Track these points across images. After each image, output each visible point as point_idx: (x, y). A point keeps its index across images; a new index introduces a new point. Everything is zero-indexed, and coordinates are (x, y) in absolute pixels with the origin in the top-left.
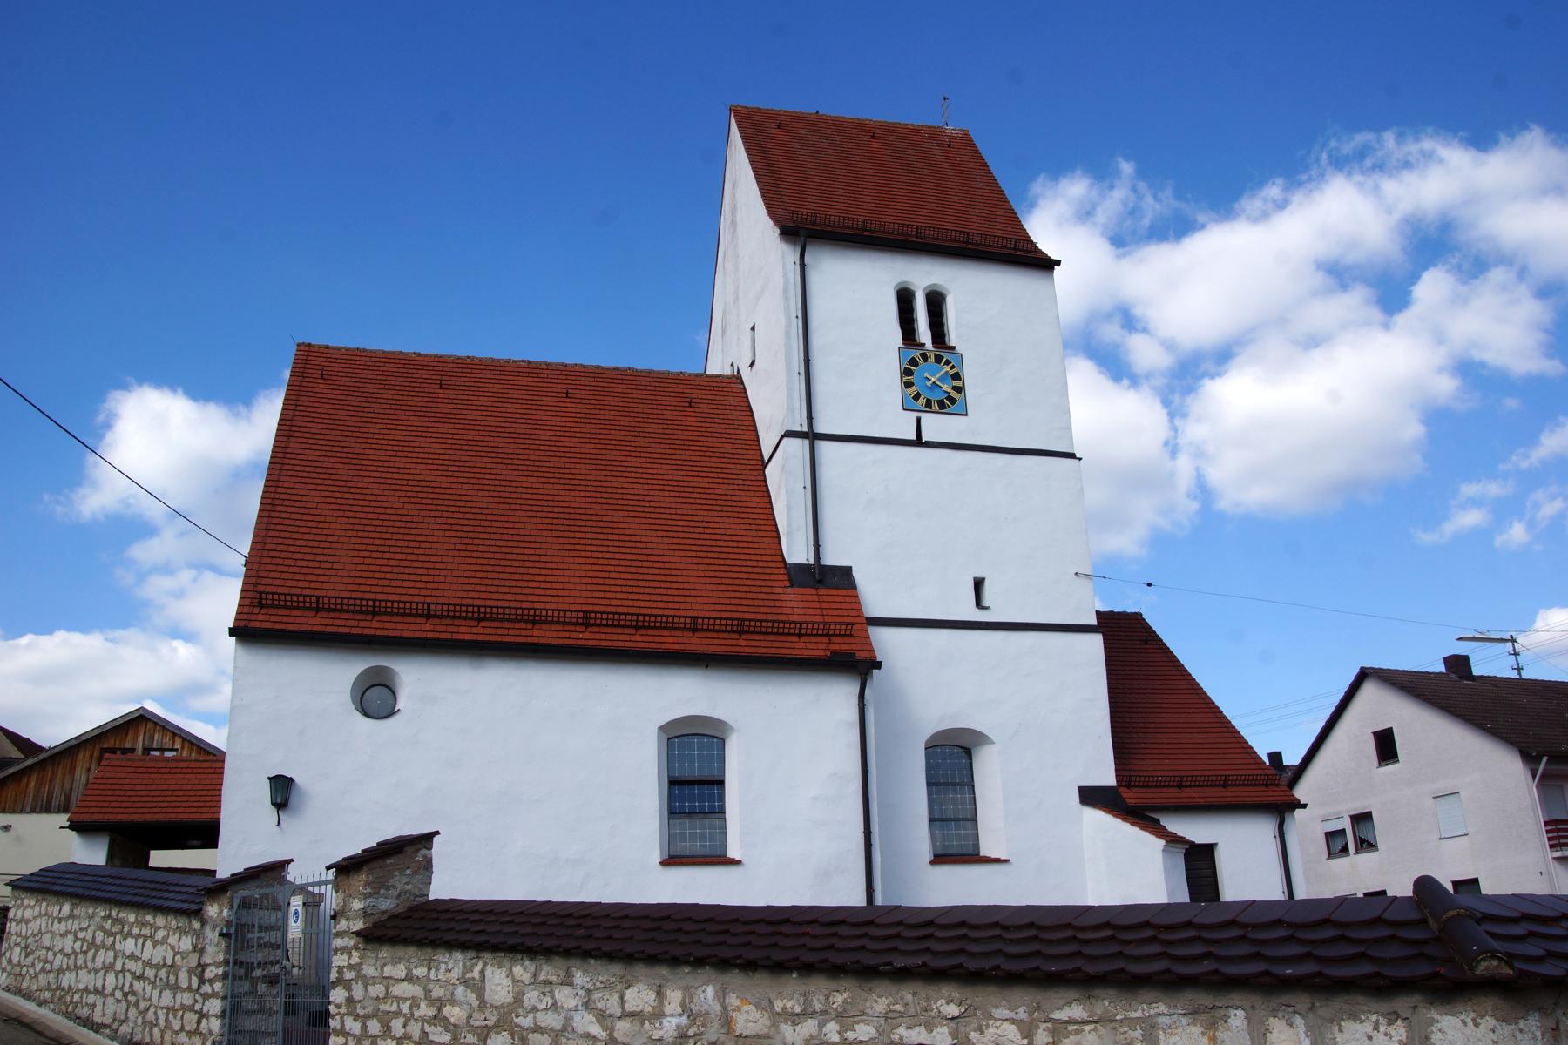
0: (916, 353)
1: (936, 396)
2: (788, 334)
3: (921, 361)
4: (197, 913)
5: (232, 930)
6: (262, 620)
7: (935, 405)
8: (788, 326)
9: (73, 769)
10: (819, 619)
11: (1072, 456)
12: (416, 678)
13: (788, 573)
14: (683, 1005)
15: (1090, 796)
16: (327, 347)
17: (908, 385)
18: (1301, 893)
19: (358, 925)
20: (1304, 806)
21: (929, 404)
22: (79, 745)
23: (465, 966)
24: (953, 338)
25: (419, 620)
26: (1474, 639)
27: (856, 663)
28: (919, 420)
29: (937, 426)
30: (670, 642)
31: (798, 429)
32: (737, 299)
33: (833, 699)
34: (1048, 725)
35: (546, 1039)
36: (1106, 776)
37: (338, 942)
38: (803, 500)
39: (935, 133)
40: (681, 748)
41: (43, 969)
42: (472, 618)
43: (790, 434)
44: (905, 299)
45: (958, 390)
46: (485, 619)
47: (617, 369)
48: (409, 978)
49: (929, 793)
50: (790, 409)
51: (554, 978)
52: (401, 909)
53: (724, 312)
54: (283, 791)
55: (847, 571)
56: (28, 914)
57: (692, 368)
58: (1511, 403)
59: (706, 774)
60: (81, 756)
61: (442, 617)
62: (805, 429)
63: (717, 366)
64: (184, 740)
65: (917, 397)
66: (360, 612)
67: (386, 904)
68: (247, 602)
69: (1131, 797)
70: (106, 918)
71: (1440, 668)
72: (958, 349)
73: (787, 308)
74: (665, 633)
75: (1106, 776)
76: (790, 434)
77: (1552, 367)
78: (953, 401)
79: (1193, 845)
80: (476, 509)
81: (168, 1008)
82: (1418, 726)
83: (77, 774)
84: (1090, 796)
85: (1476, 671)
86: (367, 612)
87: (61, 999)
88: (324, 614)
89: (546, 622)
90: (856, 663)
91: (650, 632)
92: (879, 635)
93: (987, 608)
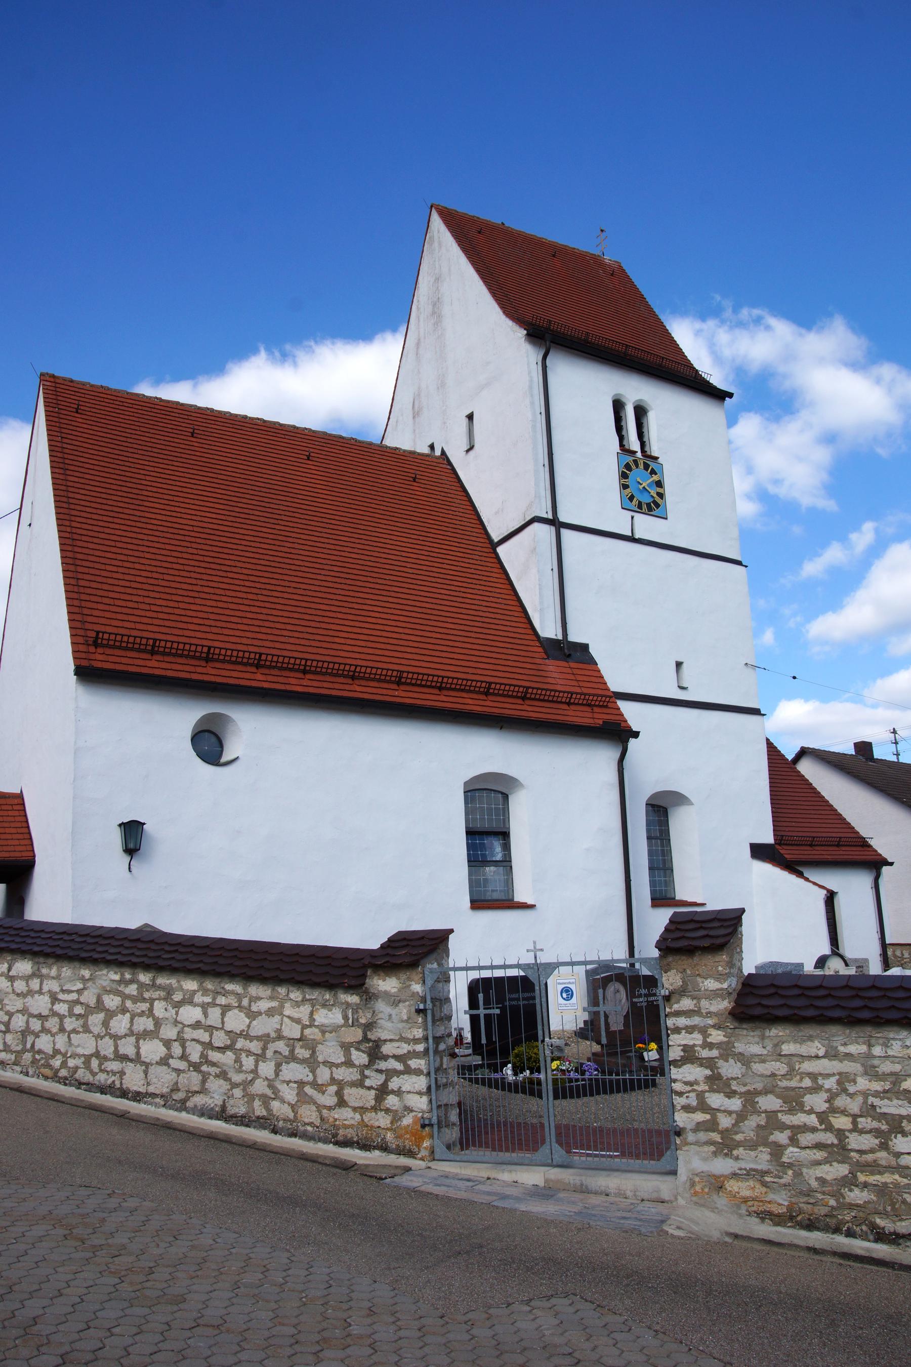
0: (630, 459)
1: (646, 499)
2: (534, 427)
3: (633, 467)
4: (357, 985)
5: (429, 1005)
6: (101, 659)
10: (578, 690)
12: (254, 730)
13: (542, 646)
15: (759, 852)
16: (72, 381)
17: (625, 487)
19: (725, 1005)
20: (891, 864)
21: (640, 505)
25: (249, 669)
29: (646, 526)
30: (471, 703)
31: (545, 516)
32: (442, 385)
33: (598, 759)
36: (767, 837)
44: (618, 406)
45: (661, 495)
46: (310, 672)
49: (649, 845)
58: (797, 530)
61: (270, 667)
62: (550, 516)
65: (631, 498)
69: (788, 853)
70: (122, 981)
73: (532, 403)
75: (767, 837)
77: (830, 505)
78: (658, 506)
81: (301, 1084)
84: (759, 852)
86: (200, 658)
90: (619, 734)
92: (622, 704)
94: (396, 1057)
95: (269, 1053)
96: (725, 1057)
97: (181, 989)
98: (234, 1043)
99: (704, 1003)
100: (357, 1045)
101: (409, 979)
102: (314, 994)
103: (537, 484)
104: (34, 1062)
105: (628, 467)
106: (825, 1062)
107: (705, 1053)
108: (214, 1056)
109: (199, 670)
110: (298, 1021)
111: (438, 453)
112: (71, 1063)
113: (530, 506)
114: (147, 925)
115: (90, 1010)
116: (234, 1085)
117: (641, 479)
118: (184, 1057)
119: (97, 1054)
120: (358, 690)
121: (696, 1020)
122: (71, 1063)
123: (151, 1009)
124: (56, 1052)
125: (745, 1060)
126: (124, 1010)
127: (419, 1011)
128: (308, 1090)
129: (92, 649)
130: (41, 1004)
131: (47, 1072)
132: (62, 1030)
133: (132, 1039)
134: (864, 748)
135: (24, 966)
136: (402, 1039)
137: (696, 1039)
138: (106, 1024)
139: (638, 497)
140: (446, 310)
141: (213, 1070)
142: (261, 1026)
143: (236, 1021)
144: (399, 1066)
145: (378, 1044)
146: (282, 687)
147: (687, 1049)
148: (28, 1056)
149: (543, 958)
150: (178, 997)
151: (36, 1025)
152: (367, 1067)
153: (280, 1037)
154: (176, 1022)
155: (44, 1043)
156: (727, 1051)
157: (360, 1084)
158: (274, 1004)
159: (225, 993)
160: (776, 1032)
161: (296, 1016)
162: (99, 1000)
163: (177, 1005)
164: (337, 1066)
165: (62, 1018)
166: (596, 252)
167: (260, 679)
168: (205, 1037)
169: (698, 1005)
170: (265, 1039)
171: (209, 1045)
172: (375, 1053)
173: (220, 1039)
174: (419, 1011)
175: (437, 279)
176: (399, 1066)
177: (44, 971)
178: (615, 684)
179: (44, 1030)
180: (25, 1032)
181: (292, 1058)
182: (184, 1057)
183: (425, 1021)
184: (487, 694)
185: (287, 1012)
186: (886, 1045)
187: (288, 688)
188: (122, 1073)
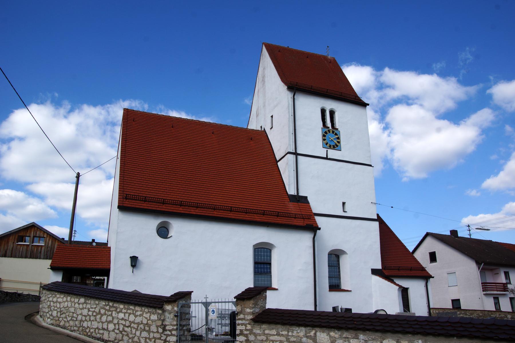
0: (327, 130)
1: (332, 144)
2: (289, 120)
4: (161, 308)
5: (179, 314)
6: (127, 203)
8: (289, 118)
9: (8, 242)
10: (300, 213)
11: (370, 166)
12: (178, 227)
15: (375, 272)
17: (324, 140)
19: (251, 317)
20: (433, 277)
21: (330, 146)
22: (11, 234)
23: (306, 331)
24: (337, 126)
26: (480, 229)
29: (332, 154)
30: (257, 218)
31: (292, 151)
34: (363, 250)
36: (379, 266)
37: (240, 322)
38: (293, 174)
39: (325, 58)
40: (258, 252)
41: (71, 320)
42: (195, 207)
43: (289, 153)
44: (323, 111)
45: (339, 142)
46: (199, 207)
47: (227, 126)
48: (278, 334)
50: (290, 145)
51: (350, 337)
52: (261, 312)
53: (258, 110)
54: (134, 261)
55: (306, 197)
56: (60, 300)
57: (241, 125)
59: (266, 261)
60: (11, 238)
61: (185, 206)
62: (294, 152)
63: (254, 126)
64: (48, 234)
65: (327, 144)
66: (159, 203)
67: (257, 310)
68: (122, 197)
69: (386, 273)
70: (106, 305)
71: (449, 233)
72: (339, 130)
73: (289, 112)
74: (255, 215)
75: (379, 266)
76: (289, 153)
78: (337, 146)
79: (404, 288)
80: (187, 171)
81: (146, 338)
82: (444, 252)
83: (9, 244)
84: (375, 272)
85: (459, 235)
86: (161, 203)
87: (84, 331)
88: (147, 203)
89: (218, 209)
90: (314, 229)
91: (250, 214)
92: (318, 219)
93: (346, 212)
94: (169, 330)
95: (139, 328)
96: (250, 334)
97: (119, 307)
98: (131, 325)
99: (246, 316)
100: (160, 326)
101: (174, 306)
102: (151, 310)
103: (289, 140)
104: (82, 330)
105: (326, 133)
106: (276, 336)
107: (245, 332)
108: (126, 329)
109: (160, 207)
110: (146, 318)
111: (263, 130)
112: (91, 330)
113: (287, 148)
114: (135, 290)
115: (98, 314)
116: (130, 338)
117: (331, 137)
118: (118, 329)
119: (98, 328)
120: (216, 213)
121: (244, 322)
122: (91, 330)
123: (112, 314)
124: (88, 327)
125: (256, 335)
126: (105, 314)
127: (175, 316)
128: (148, 340)
129: (125, 200)
130: (85, 312)
131: (85, 333)
132: (90, 320)
133: (106, 323)
134: (454, 233)
135: (82, 300)
136: (171, 325)
137: (243, 328)
138: (101, 318)
139: (329, 143)
140: (266, 79)
141: (125, 333)
142: (138, 320)
143: (132, 318)
144: (170, 333)
145: (165, 326)
146: (188, 212)
147: (241, 331)
148: (81, 328)
149: (209, 300)
150: (118, 310)
151: (84, 318)
152: (162, 333)
153: (142, 323)
154: (118, 318)
155: (85, 324)
156: (251, 332)
157: (160, 339)
158: (141, 313)
159: (130, 309)
160: (264, 326)
161: (146, 317)
162: (100, 311)
163: (118, 313)
164: (155, 333)
165: (90, 316)
166: (325, 54)
167: (181, 210)
168: (124, 323)
169: (244, 317)
170: (138, 324)
171: (125, 326)
172: (164, 330)
173: (128, 324)
174: (175, 316)
175: (264, 69)
176: (170, 333)
177: (87, 302)
178: (315, 211)
179: (86, 320)
180: (81, 321)
181: (144, 330)
182: (118, 329)
183: (177, 319)
184: (264, 215)
185: (144, 315)
186: (292, 332)
187: (190, 213)
188: (103, 334)
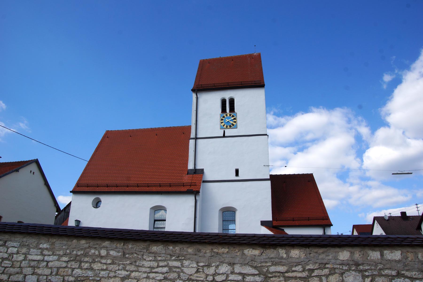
6: (78, 189)
7: (228, 127)
11: (266, 135)
12: (105, 199)
14: (105, 259)
18: (197, 231)
21: (227, 127)
27: (193, 191)
28: (224, 131)
29: (229, 132)
30: (154, 189)
33: (190, 200)
35: (118, 279)
36: (269, 217)
59: (163, 218)
69: (275, 223)
75: (269, 217)
78: (233, 125)
